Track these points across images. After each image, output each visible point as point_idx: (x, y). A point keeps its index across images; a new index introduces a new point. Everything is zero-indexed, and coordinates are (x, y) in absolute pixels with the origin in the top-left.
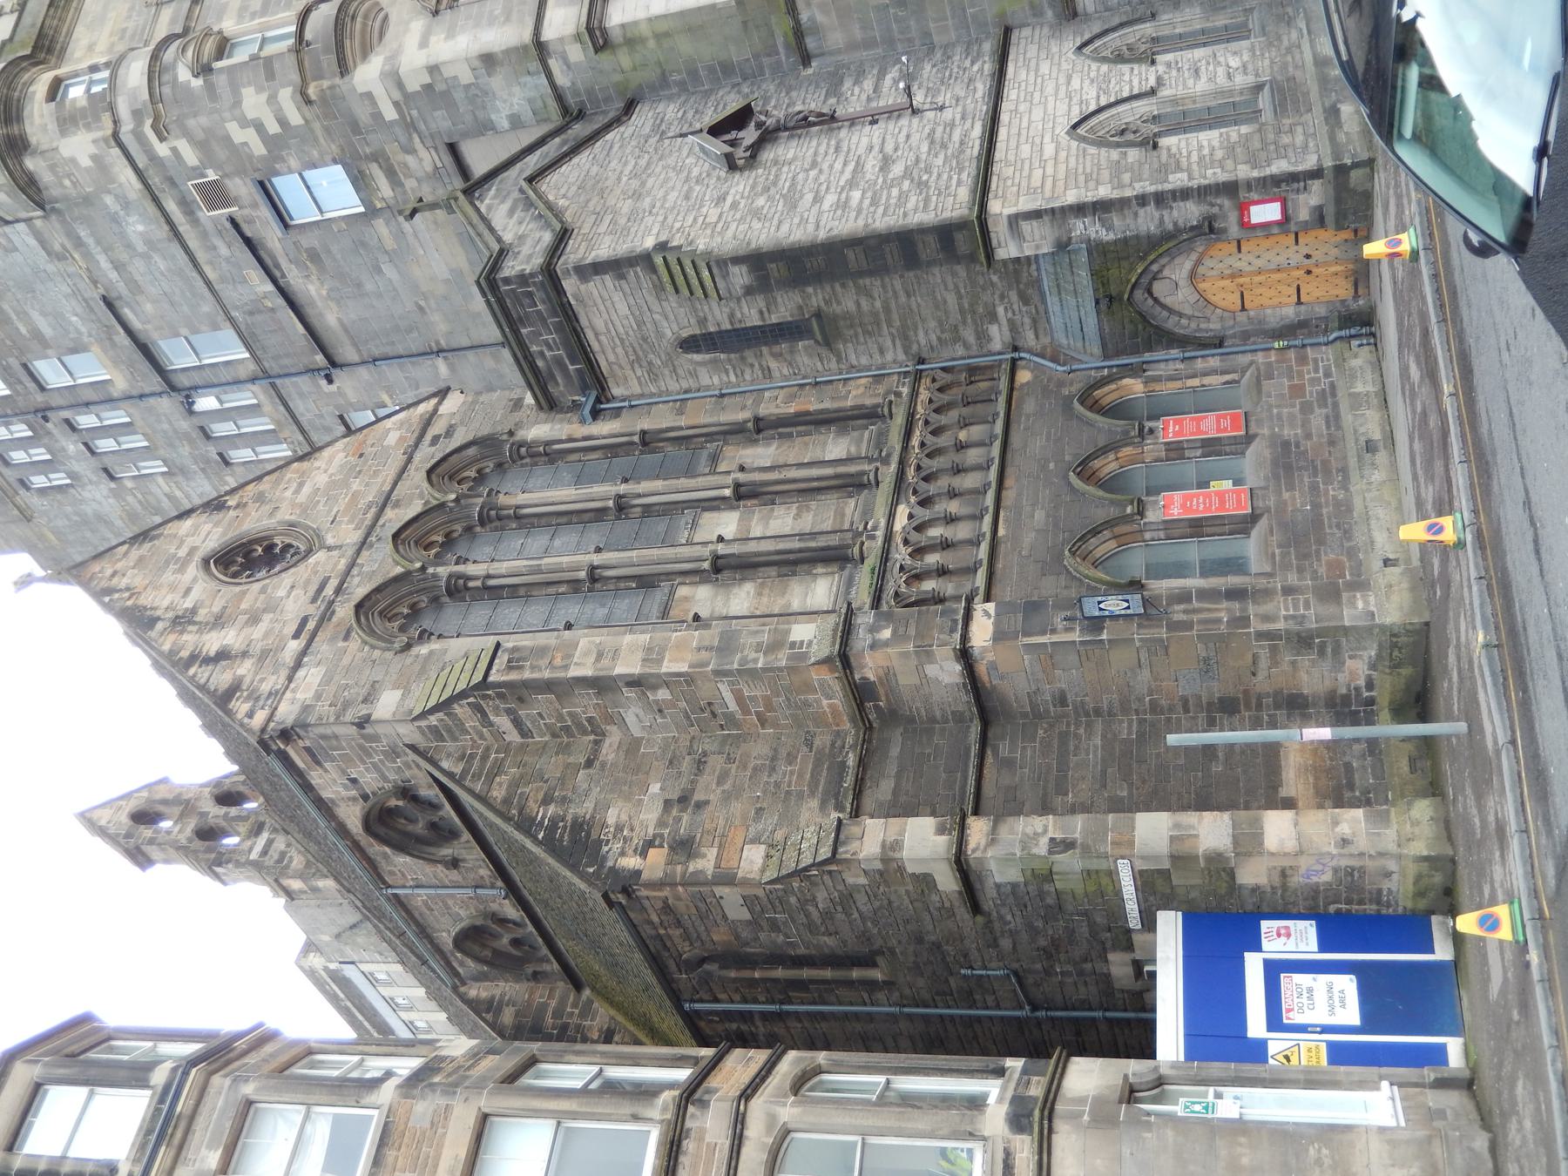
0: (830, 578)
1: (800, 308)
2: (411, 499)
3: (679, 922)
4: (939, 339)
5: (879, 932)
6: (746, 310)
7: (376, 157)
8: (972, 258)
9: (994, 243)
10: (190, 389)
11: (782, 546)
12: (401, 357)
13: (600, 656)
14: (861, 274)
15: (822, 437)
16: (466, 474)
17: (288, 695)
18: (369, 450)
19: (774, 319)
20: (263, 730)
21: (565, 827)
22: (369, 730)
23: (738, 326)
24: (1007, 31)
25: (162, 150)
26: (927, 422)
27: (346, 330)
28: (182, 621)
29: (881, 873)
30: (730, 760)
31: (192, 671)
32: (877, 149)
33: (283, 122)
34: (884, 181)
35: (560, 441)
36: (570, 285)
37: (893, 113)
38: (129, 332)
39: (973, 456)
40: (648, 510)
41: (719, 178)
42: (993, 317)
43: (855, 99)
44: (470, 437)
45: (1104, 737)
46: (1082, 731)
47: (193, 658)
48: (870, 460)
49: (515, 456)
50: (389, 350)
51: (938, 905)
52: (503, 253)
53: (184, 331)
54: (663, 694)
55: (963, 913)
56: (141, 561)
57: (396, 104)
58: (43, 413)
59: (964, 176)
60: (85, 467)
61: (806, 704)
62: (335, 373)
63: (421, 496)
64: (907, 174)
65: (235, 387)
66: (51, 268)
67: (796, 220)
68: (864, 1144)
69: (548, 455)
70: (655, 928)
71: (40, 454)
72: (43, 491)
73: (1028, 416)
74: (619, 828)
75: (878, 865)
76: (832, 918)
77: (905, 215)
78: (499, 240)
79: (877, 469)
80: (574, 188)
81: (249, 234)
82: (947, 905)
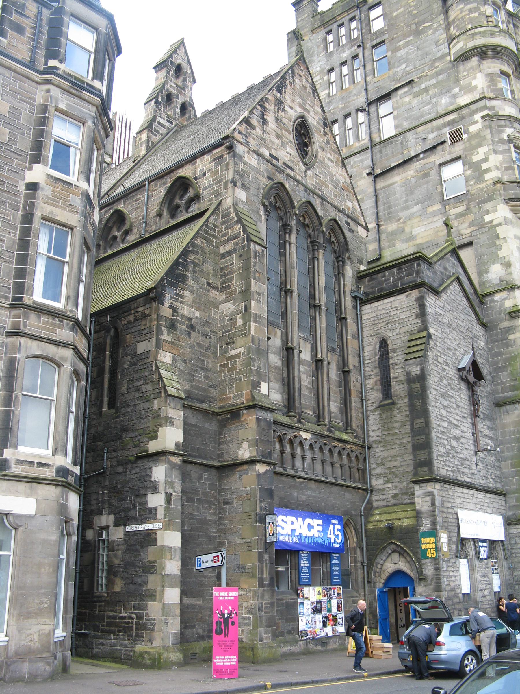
0: (281, 401)
1: (397, 396)
2: (324, 209)
3: (137, 320)
4: (379, 457)
5: (127, 412)
6: (398, 371)
7: (468, 208)
8: (416, 474)
9: (422, 485)
10: (368, 111)
11: (296, 379)
12: (377, 207)
13: (259, 294)
14: (412, 425)
15: (339, 401)
16: (332, 236)
17: (247, 149)
18: (345, 193)
19: (393, 383)
20: (233, 138)
21: (183, 271)
22: (230, 185)
23: (391, 366)
24: (504, 495)
25: (477, 117)
26: (344, 449)
27: (391, 185)
28: (279, 104)
29: (159, 416)
30: (207, 349)
31: (259, 107)
32: (463, 435)
33: (487, 170)
34: (450, 437)
35: (344, 281)
36: (415, 294)
37: (476, 443)
38: (397, 89)
39: (328, 469)
40: (313, 319)
41: (455, 363)
42: (387, 482)
43: (483, 426)
44: (348, 240)
45: (210, 520)
46: (212, 511)
47: (264, 108)
48: (330, 422)
49: (339, 259)
50: (380, 203)
51: (141, 440)
52: (430, 264)
53: (395, 113)
54: (240, 322)
55: (135, 452)
56: (304, 88)
57: (491, 222)
58: (361, 46)
59: (450, 473)
60: (336, 61)
61: (231, 387)
62: (371, 178)
63: (325, 215)
64: (453, 448)
65: (368, 131)
66: (427, 60)
67: (437, 397)
68: (51, 400)
69: (339, 275)
70: (135, 309)
71: (344, 41)
72: (325, 39)
73: (344, 495)
74: (182, 297)
75: (163, 415)
76: (136, 391)
77: (437, 446)
78: (436, 262)
79: (326, 425)
80: (453, 298)
81: (438, 148)
82: (141, 444)
